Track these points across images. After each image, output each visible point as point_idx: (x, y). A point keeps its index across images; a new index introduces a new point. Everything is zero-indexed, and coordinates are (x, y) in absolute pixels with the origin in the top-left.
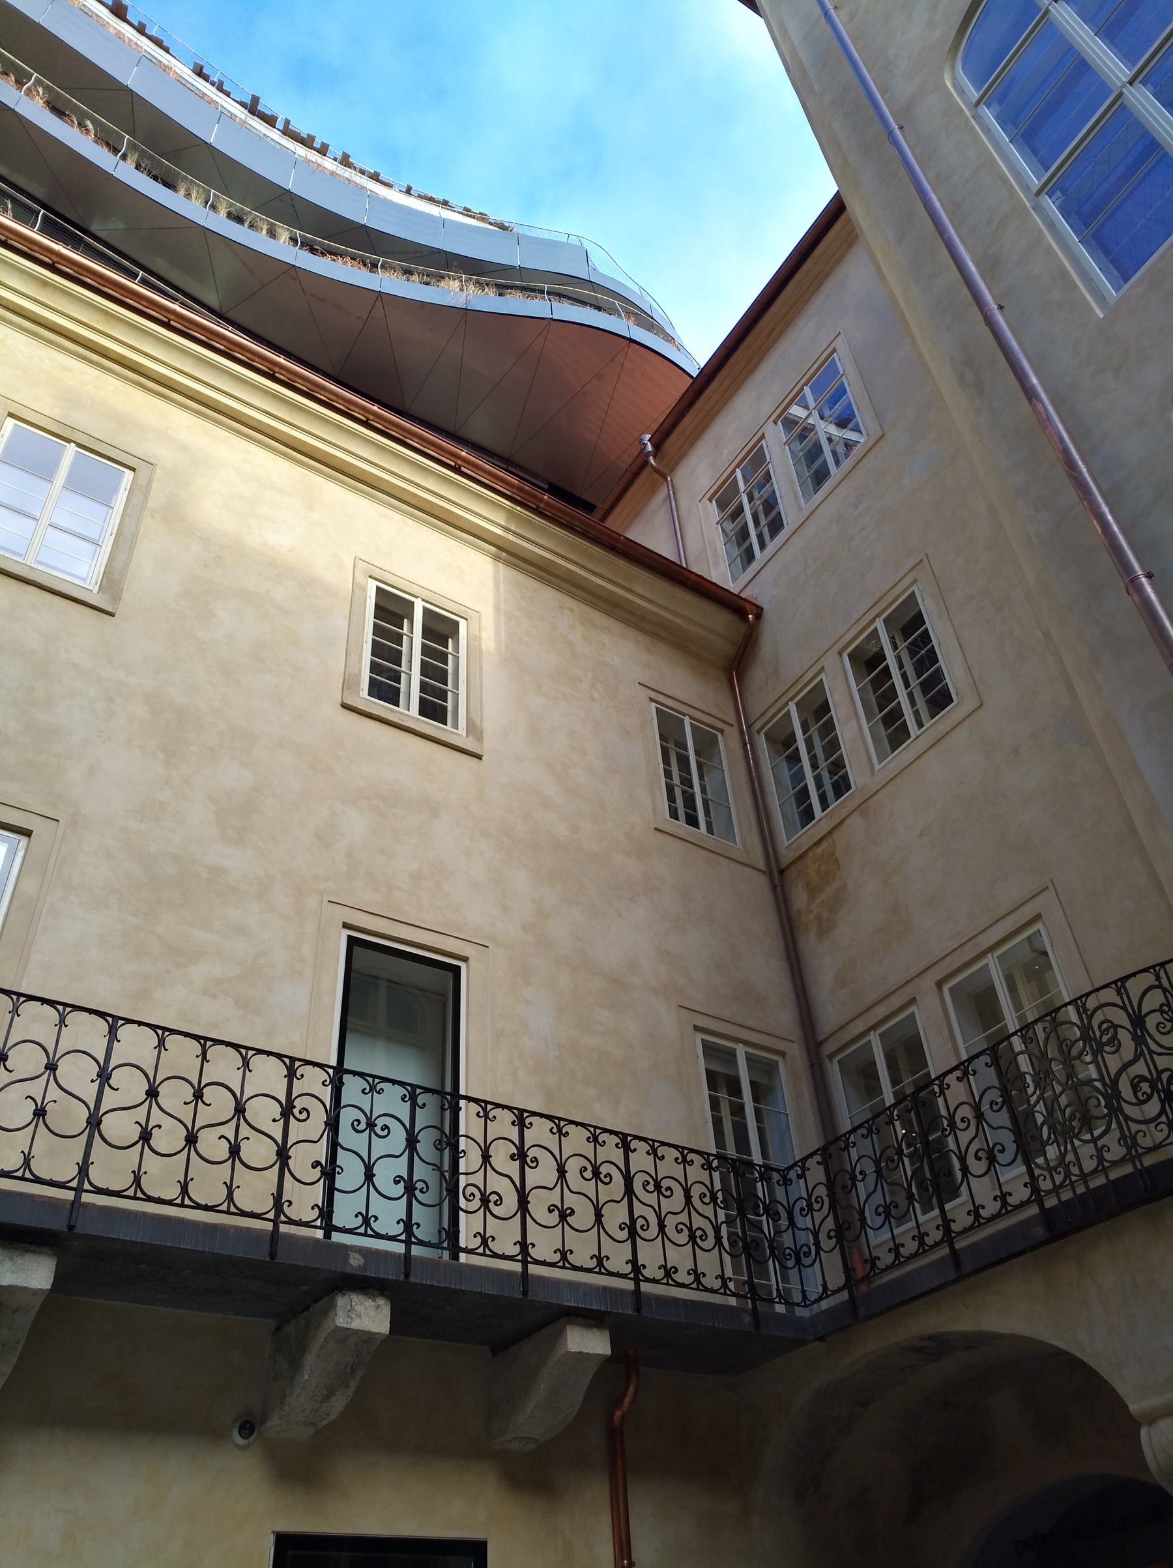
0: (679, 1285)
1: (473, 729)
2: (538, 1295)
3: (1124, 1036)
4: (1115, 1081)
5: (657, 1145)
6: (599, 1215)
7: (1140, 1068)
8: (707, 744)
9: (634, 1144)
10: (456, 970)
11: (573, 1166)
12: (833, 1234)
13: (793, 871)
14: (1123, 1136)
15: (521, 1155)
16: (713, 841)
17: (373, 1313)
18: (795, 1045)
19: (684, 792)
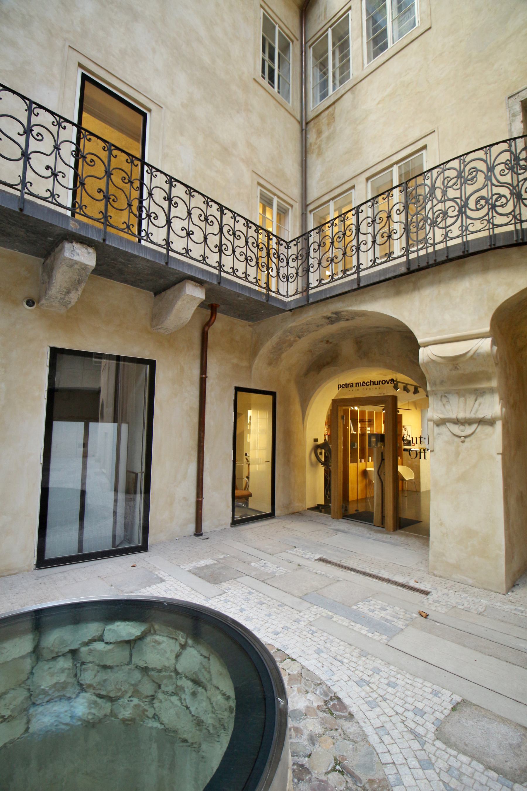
0: (238, 277)
2: (173, 266)
3: (481, 178)
4: (467, 199)
6: (205, 239)
7: (484, 193)
8: (285, 48)
9: (226, 211)
10: (145, 115)
11: (195, 213)
12: (305, 269)
13: (312, 124)
14: (462, 226)
15: (169, 199)
16: (279, 97)
17: (86, 255)
18: (297, 204)
19: (269, 66)
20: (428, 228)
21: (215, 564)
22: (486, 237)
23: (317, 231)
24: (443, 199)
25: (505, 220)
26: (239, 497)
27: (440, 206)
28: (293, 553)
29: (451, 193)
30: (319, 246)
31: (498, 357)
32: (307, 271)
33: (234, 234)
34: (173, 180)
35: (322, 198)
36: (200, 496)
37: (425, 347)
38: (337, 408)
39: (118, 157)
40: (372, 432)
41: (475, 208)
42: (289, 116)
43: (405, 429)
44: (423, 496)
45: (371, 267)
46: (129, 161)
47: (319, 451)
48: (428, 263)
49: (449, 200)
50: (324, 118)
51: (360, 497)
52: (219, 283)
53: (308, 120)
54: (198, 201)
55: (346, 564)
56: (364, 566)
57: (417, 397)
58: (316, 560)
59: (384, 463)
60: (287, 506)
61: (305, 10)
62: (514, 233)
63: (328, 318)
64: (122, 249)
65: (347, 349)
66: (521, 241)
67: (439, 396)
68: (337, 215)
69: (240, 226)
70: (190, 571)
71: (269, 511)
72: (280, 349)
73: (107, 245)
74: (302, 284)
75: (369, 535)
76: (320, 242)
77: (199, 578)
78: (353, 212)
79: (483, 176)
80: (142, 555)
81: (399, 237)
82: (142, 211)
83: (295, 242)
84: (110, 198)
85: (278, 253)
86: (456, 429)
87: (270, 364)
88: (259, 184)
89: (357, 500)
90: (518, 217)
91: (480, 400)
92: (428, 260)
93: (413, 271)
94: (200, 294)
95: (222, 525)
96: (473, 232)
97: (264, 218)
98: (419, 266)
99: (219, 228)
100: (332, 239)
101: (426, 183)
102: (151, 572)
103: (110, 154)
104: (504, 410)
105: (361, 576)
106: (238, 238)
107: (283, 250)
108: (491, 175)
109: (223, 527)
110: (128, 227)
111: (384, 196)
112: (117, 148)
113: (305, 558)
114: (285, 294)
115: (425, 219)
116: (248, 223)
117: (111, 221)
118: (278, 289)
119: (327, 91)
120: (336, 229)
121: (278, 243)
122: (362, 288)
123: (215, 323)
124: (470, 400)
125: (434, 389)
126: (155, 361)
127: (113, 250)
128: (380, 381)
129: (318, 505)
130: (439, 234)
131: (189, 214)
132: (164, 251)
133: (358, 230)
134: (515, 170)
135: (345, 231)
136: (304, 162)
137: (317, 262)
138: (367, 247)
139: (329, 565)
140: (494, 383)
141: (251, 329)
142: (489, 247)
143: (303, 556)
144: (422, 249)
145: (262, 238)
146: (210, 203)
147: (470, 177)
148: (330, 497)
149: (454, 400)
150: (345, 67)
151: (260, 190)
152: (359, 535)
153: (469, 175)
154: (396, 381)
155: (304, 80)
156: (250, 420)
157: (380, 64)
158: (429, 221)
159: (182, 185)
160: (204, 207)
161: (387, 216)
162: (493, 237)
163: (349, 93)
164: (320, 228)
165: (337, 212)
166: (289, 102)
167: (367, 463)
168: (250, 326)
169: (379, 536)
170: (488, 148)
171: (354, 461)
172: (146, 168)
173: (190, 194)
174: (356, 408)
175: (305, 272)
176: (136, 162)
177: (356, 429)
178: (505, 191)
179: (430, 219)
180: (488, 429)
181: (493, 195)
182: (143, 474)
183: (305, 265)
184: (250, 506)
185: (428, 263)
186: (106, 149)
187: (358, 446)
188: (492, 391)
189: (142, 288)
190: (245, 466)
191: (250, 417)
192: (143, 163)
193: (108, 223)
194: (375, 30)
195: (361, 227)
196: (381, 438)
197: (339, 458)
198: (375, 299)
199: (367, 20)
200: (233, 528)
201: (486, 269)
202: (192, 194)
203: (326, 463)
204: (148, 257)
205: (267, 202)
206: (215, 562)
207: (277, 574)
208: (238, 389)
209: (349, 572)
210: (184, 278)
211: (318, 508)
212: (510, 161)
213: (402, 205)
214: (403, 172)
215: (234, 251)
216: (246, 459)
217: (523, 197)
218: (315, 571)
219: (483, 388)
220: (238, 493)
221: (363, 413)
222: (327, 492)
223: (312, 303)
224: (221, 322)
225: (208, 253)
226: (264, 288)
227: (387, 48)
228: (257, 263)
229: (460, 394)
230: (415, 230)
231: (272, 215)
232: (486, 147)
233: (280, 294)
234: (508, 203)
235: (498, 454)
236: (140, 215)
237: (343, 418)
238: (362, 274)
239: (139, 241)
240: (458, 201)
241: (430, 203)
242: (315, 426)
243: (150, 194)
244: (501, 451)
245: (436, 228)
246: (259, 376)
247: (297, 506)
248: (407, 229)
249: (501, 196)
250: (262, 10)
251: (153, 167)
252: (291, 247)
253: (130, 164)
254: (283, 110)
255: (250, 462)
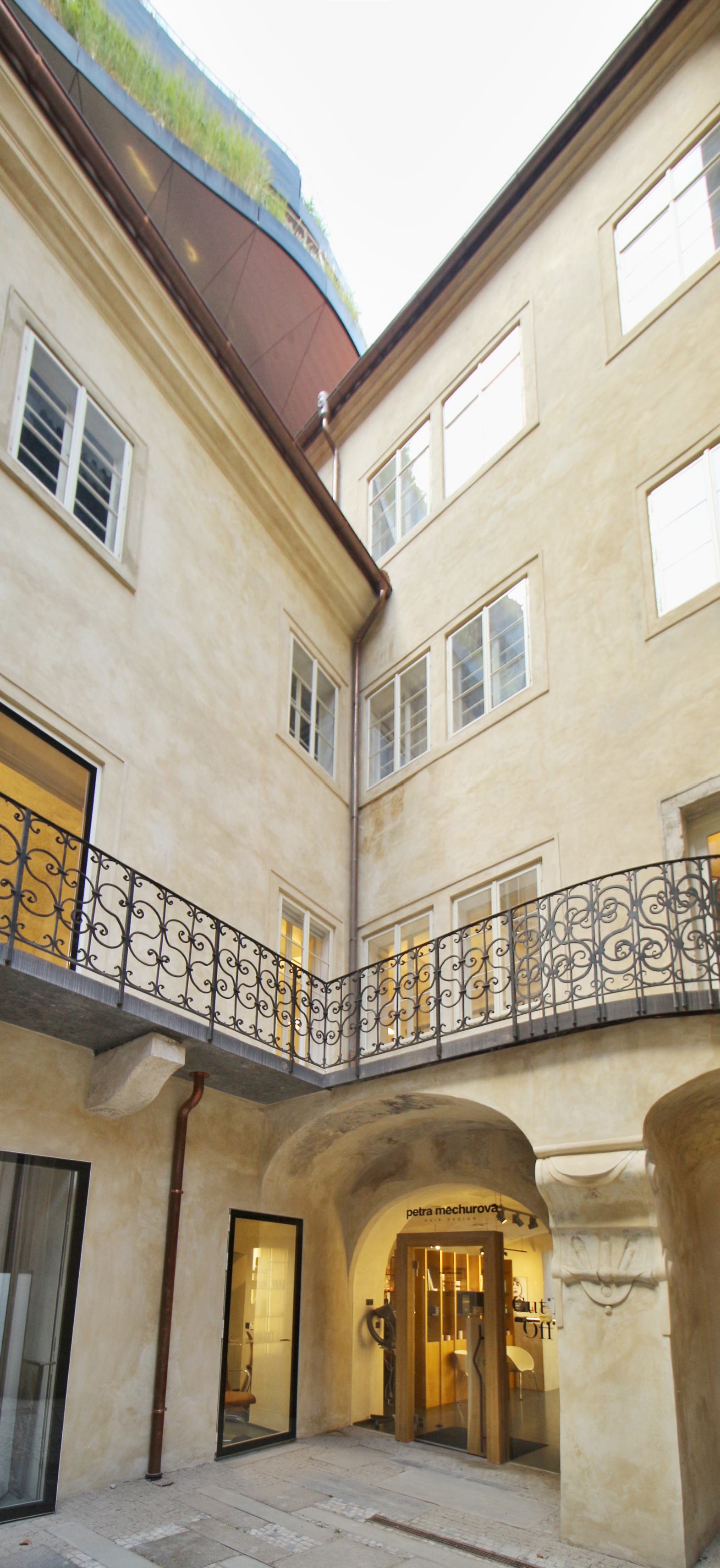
1: (127, 557)
2: (130, 1009)
3: (622, 912)
4: (603, 943)
5: (242, 936)
6: (189, 970)
7: (627, 936)
8: (327, 695)
10: (93, 771)
11: (173, 930)
13: (367, 811)
14: (596, 981)
16: (317, 765)
20: (545, 979)
21: (182, 1534)
22: (632, 1000)
23: (374, 969)
24: (567, 939)
25: (659, 977)
26: (233, 1400)
27: (562, 950)
28: (327, 1507)
29: (579, 932)
30: (377, 992)
31: (658, 1181)
32: (357, 1029)
33: (238, 965)
34: (136, 876)
35: (383, 919)
36: (161, 1404)
37: (544, 1158)
38: (406, 1250)
39: (40, 833)
40: (463, 1290)
41: (614, 957)
42: (332, 795)
43: (518, 1283)
44: (548, 1399)
45: (458, 1030)
46: (61, 840)
47: (375, 1320)
48: (546, 1031)
49: (576, 941)
50: (386, 804)
51: (444, 1402)
52: (210, 1041)
53: (362, 804)
54: (178, 910)
55: (420, 1527)
56: (452, 1529)
57: (534, 1232)
58: (367, 1520)
59: (483, 1344)
60: (317, 1420)
61: (360, 643)
62: (674, 997)
63: (391, 1104)
64: (40, 977)
65: (422, 1153)
66: (684, 1010)
67: (569, 1238)
68: (406, 949)
69: (248, 953)
70: (134, 1550)
71: (285, 1429)
72: (311, 1150)
73: (13, 971)
74: (349, 1047)
75: (459, 1472)
76: (379, 987)
77: (151, 1564)
78: (431, 946)
79: (626, 911)
80: (42, 1521)
81: (501, 989)
82: (81, 920)
83: (337, 984)
84: (23, 896)
85: (310, 998)
86: (598, 1293)
87: (293, 1172)
88: (281, 891)
89: (440, 1406)
90: (679, 975)
91: (633, 1246)
92: (546, 1027)
93: (524, 1042)
94: (176, 1057)
95: (198, 1458)
96: (612, 992)
97: (289, 943)
98: (532, 1034)
99: (214, 955)
100: (398, 984)
101: (541, 913)
102: (59, 1554)
103: (28, 826)
104: (670, 1264)
105: (446, 1548)
106: (245, 971)
107: (318, 994)
108: (637, 912)
109: (201, 1462)
110: (54, 943)
111: (479, 927)
112: (41, 819)
113: (348, 1518)
114: (321, 1062)
115: (541, 966)
116: (261, 949)
117: (24, 933)
118: (309, 1054)
119: (392, 765)
120: (404, 969)
121: (311, 983)
122: (445, 1062)
123: (201, 1104)
124: (618, 1244)
125: (560, 1226)
126: (89, 1165)
127: (23, 979)
128: (474, 1208)
129: (372, 1416)
130: (562, 990)
131: (163, 929)
132: (116, 985)
133: (438, 974)
134: (673, 906)
135: (418, 972)
136: (354, 864)
137: (374, 1017)
138: (453, 1000)
139: (390, 1529)
140: (653, 1221)
141: (262, 1114)
142: (636, 1015)
143: (345, 1513)
144: (535, 1009)
145: (285, 974)
146: (200, 916)
147: (606, 911)
148: (393, 1401)
149: (592, 1244)
150: (419, 733)
151: (284, 900)
152: (442, 1472)
153: (605, 908)
154: (501, 1207)
155: (355, 745)
156: (257, 1264)
157: (473, 735)
158: (546, 970)
159: (152, 885)
160: (188, 921)
161: (482, 956)
162: (642, 1001)
163: (425, 771)
164: (379, 966)
165: (406, 942)
166: (332, 774)
167: (457, 1341)
168: (261, 1110)
169: (477, 1472)
170: (631, 872)
171: (434, 1337)
172: (91, 853)
173: (166, 899)
174: (438, 1248)
175: (353, 1030)
176: (73, 843)
177: (436, 1283)
178: (658, 936)
179: (548, 966)
180: (646, 1294)
181: (640, 940)
182: (54, 1367)
183: (353, 1019)
184: (253, 1419)
185: (546, 1031)
186: (21, 818)
187: (441, 1311)
188: (649, 1233)
189: (74, 1041)
190: (246, 1347)
191: (257, 1259)
192: (87, 846)
193: (16, 935)
194: (465, 686)
195: (442, 969)
196: (478, 1299)
197: (409, 1333)
198: (464, 1079)
199: (454, 670)
200: (219, 1463)
201: (633, 1046)
202: (170, 899)
203: (387, 1343)
204: (86, 993)
205: (294, 919)
206: (184, 1530)
207: (296, 1550)
208: (236, 1214)
209: (425, 1541)
210: (148, 1030)
211: (372, 1422)
212: (665, 893)
213: (506, 943)
214: (507, 892)
215: (236, 992)
216: (248, 1334)
217: (685, 946)
218: (365, 1541)
219: (636, 1229)
220: (230, 1396)
221: (448, 1257)
222: (388, 1392)
223: (366, 1080)
224: (212, 1101)
225: (192, 992)
226: (286, 1051)
227: (483, 713)
228: (275, 1012)
229: (602, 1235)
230: (525, 981)
231: (301, 938)
232: (628, 871)
233: (313, 1063)
234: (664, 954)
235: (665, 1336)
236: (77, 926)
237: (415, 1266)
238: (444, 1040)
239: (73, 967)
240: (590, 944)
241: (547, 944)
242: (368, 1279)
243: (96, 895)
244: (669, 1332)
245: (557, 980)
246: (274, 1191)
247: (336, 1419)
248: (513, 978)
249: (652, 942)
250: (292, 636)
251: (102, 853)
252: (331, 991)
253: (64, 845)
254: (322, 785)
255: (255, 1340)
